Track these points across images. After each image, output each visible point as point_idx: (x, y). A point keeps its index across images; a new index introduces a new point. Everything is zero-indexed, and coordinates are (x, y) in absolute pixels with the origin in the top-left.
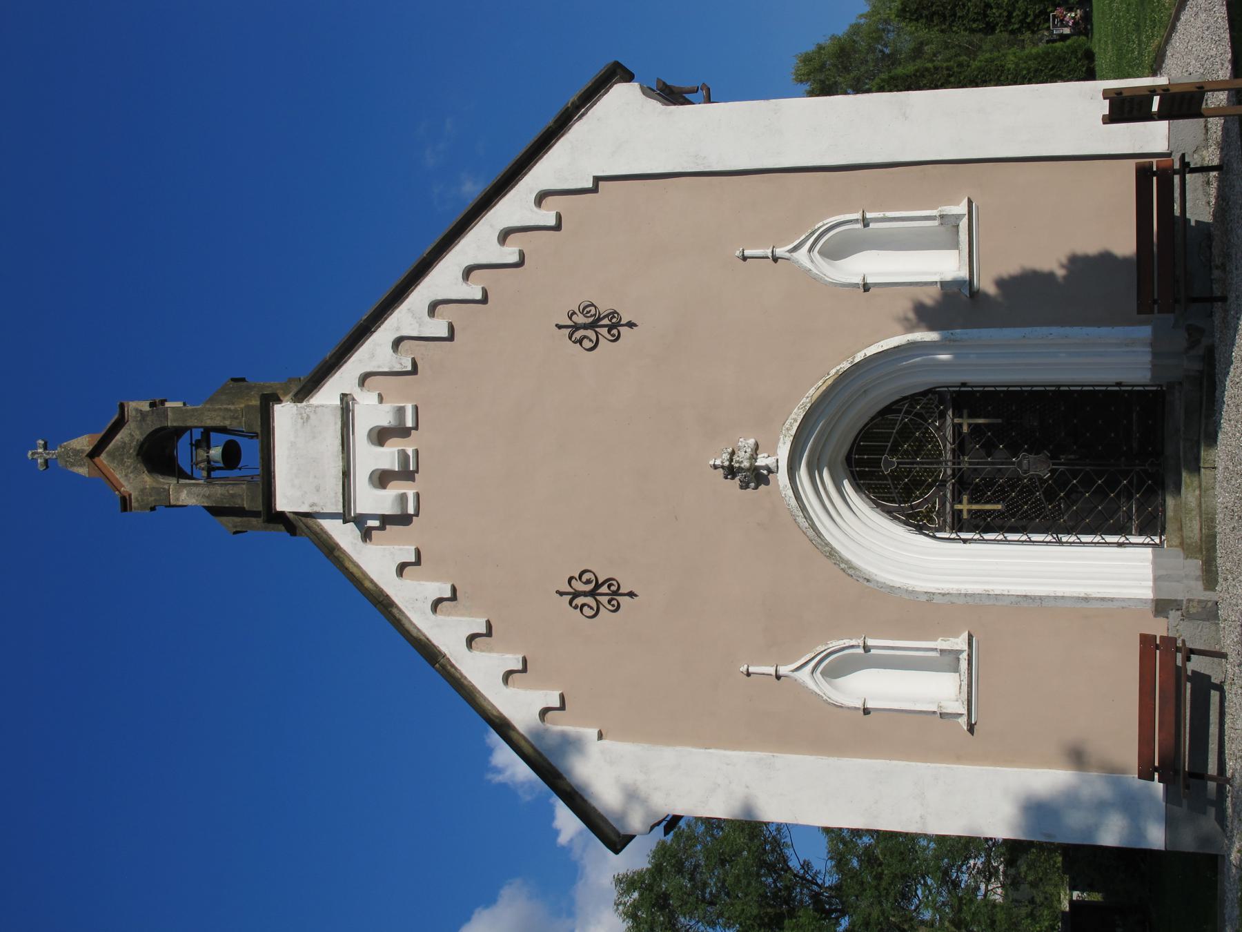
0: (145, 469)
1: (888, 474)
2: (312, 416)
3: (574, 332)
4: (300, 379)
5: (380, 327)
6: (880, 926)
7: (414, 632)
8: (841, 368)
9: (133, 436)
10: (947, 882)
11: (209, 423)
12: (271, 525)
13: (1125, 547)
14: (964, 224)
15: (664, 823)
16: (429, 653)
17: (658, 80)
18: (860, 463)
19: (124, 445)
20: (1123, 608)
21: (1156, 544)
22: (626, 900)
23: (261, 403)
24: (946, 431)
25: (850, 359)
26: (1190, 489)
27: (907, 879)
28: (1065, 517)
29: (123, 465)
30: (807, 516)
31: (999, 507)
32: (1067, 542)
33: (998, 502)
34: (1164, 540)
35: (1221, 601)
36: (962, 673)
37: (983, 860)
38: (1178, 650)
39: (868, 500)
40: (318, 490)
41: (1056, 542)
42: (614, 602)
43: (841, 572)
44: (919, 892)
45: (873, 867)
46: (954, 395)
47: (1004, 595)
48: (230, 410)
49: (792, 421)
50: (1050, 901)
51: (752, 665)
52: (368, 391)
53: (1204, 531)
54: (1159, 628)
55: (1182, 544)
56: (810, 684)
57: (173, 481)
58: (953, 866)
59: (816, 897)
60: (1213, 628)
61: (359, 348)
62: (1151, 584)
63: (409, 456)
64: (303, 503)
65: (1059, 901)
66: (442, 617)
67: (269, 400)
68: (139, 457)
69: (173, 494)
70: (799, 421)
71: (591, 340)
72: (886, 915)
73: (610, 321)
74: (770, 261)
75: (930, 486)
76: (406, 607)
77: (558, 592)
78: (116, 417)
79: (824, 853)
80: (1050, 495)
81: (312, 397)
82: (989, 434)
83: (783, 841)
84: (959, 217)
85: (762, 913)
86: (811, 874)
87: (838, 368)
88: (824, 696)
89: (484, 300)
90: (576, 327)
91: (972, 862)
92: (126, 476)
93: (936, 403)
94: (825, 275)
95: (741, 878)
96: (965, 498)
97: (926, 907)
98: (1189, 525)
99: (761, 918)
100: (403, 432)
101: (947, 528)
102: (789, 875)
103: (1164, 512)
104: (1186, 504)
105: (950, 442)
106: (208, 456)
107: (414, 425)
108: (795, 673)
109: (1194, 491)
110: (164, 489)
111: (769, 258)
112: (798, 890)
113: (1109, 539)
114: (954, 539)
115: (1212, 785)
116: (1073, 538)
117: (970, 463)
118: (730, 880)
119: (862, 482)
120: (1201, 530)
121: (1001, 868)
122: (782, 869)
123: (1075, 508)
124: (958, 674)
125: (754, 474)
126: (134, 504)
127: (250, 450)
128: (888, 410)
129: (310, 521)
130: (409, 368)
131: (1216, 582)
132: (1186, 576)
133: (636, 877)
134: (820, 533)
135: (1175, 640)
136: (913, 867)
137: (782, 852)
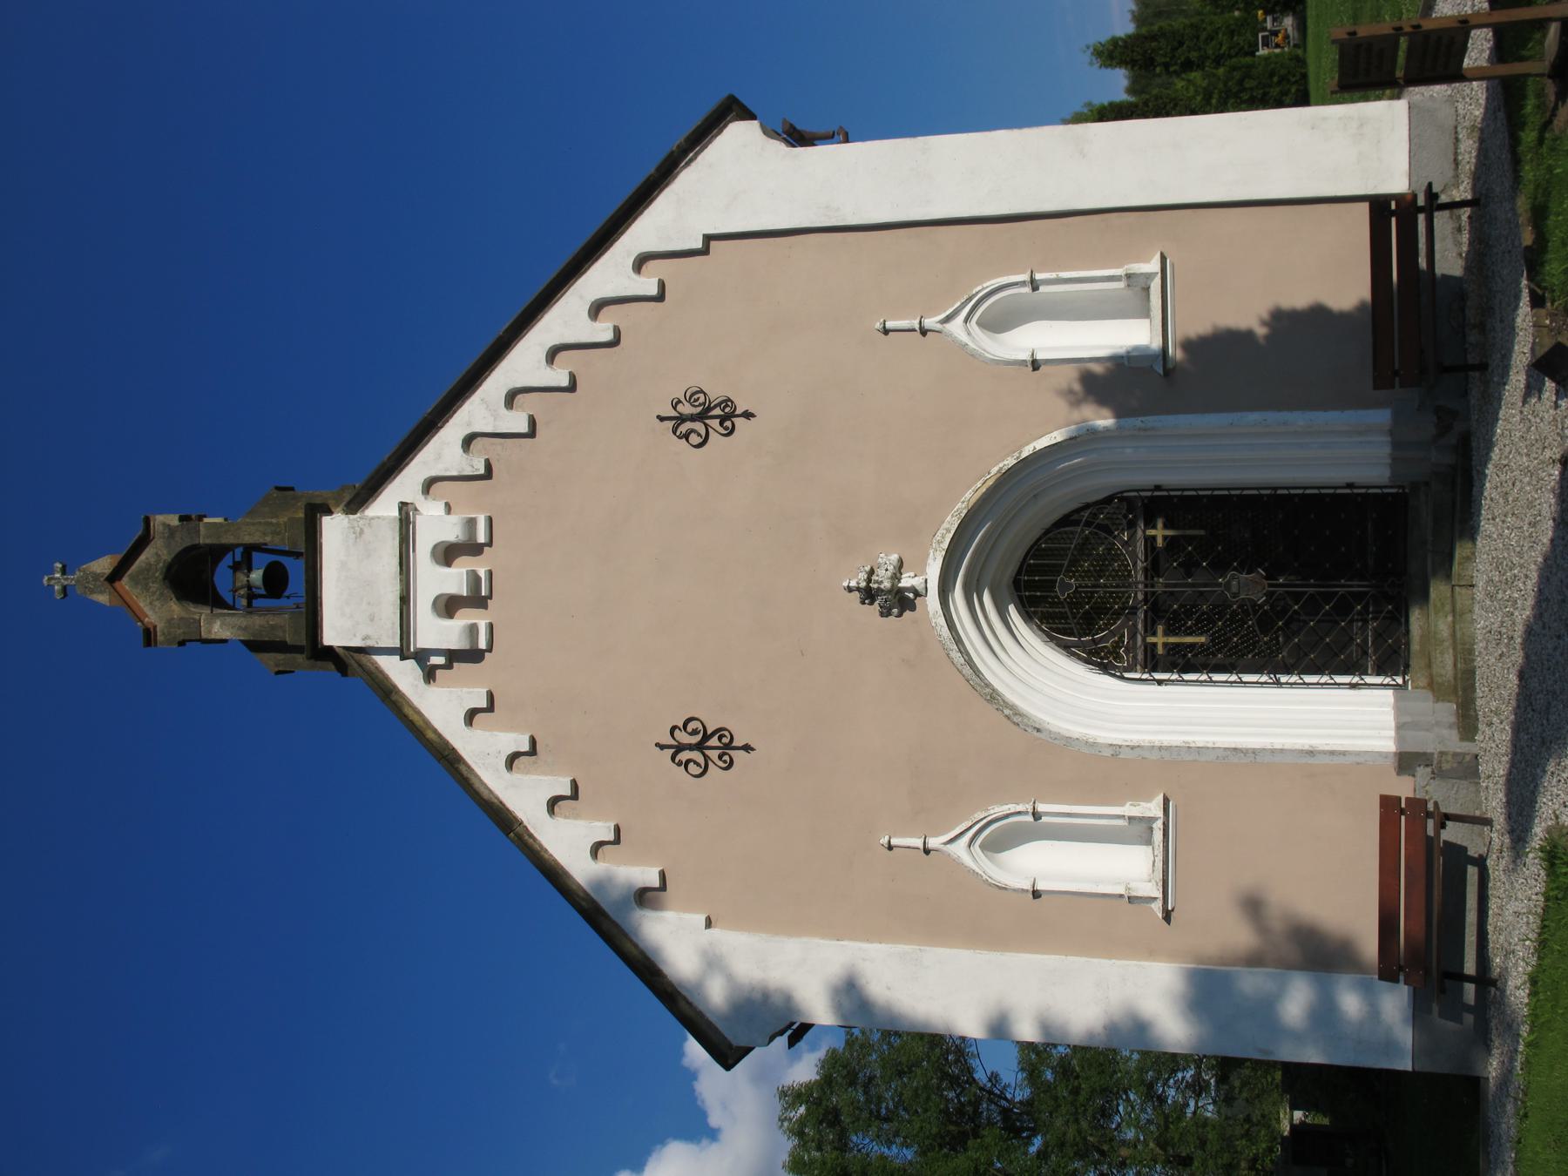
0: (173, 596)
1: (1065, 599)
2: (366, 530)
3: (679, 425)
4: (355, 487)
5: (448, 421)
6: (1076, 1148)
7: (485, 794)
8: (1005, 465)
9: (159, 556)
10: (1152, 1097)
11: (247, 540)
12: (319, 663)
13: (1360, 689)
14: (1156, 285)
15: (789, 1032)
16: (502, 819)
17: (785, 121)
18: (1030, 585)
19: (149, 567)
20: (1358, 764)
21: (1398, 685)
22: (792, 1115)
23: (306, 515)
24: (1135, 547)
25: (1016, 454)
26: (1441, 614)
27: (1111, 1092)
28: (1284, 653)
29: (148, 590)
30: (962, 649)
31: (1202, 639)
32: (1287, 683)
33: (1201, 634)
34: (1408, 680)
35: (1482, 753)
36: (1156, 847)
37: (1193, 1073)
38: (1429, 815)
39: (1040, 633)
40: (372, 620)
41: (1274, 683)
42: (726, 758)
43: (1005, 720)
44: (1121, 1108)
45: (1068, 1080)
46: (1146, 501)
47: (1208, 748)
48: (271, 523)
49: (945, 532)
50: (1268, 1121)
51: (895, 836)
52: (434, 500)
53: (1459, 665)
54: (1404, 788)
55: (1431, 685)
56: (966, 859)
57: (206, 611)
58: (1158, 1079)
59: (1005, 1113)
60: (1472, 789)
61: (422, 448)
62: (1392, 733)
63: (481, 578)
64: (355, 635)
65: (1278, 1120)
66: (519, 776)
67: (315, 512)
68: (166, 581)
69: (204, 626)
70: (953, 532)
71: (699, 435)
72: (1083, 1135)
73: (723, 411)
74: (918, 334)
75: (1118, 614)
76: (476, 763)
77: (657, 745)
78: (140, 533)
79: (1014, 1066)
80: (1265, 624)
81: (367, 508)
82: (1190, 548)
83: (967, 1050)
84: (1149, 276)
85: (942, 1131)
86: (999, 1088)
87: (1001, 465)
88: (983, 874)
89: (572, 387)
90: (682, 419)
91: (1180, 1075)
92: (151, 603)
93: (1124, 511)
94: (985, 350)
95: (920, 1092)
96: (1160, 629)
97: (1129, 1126)
98: (1440, 659)
99: (942, 1137)
100: (473, 549)
101: (1139, 667)
102: (974, 1089)
103: (1408, 644)
104: (1435, 633)
105: (1141, 561)
106: (248, 581)
107: (488, 541)
108: (948, 846)
109: (1446, 616)
110: (193, 619)
111: (915, 331)
112: (985, 1106)
113: (1339, 679)
114: (1146, 680)
115: (1470, 990)
116: (1294, 679)
117: (1167, 586)
118: (907, 1094)
119: (1032, 609)
120: (1455, 665)
121: (1212, 1081)
122: (967, 1082)
123: (1296, 640)
124: (1151, 847)
125: (897, 597)
126: (160, 638)
127: (295, 568)
128: (1066, 520)
129: (363, 658)
130: (482, 471)
131: (1475, 730)
132: (1438, 724)
133: (803, 1090)
134: (979, 671)
135: (1425, 802)
136: (1114, 1080)
137: (966, 1063)
